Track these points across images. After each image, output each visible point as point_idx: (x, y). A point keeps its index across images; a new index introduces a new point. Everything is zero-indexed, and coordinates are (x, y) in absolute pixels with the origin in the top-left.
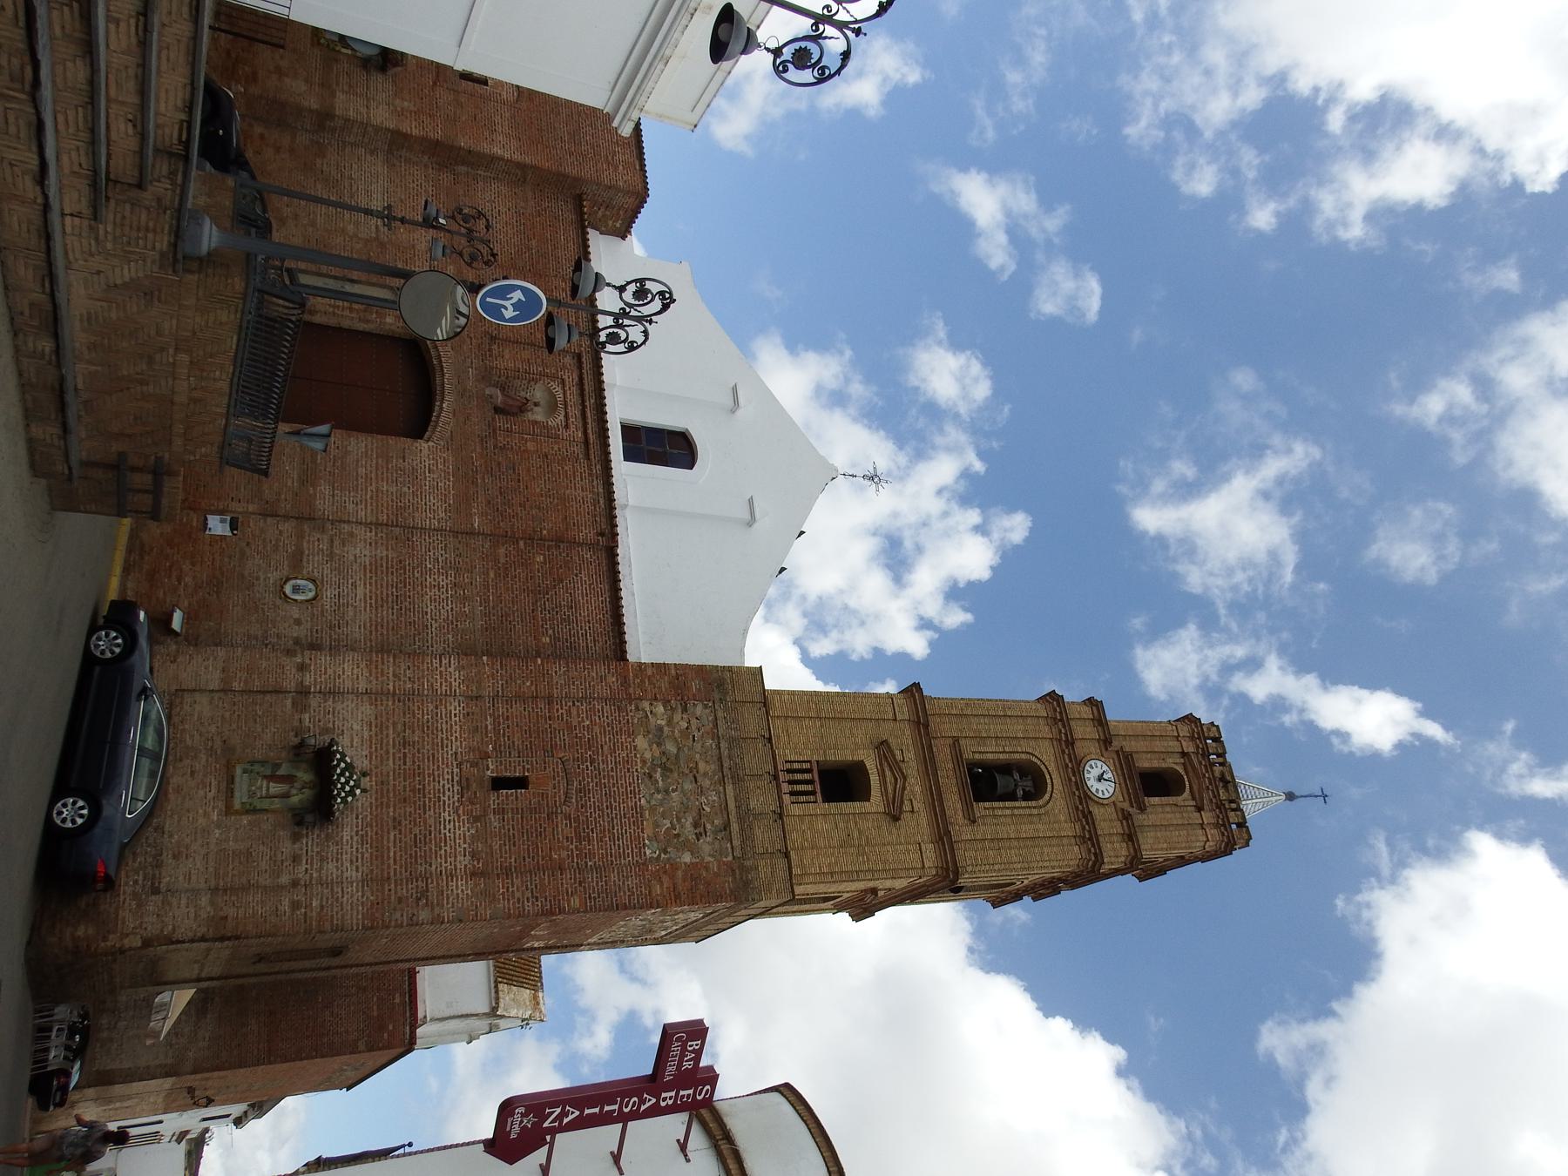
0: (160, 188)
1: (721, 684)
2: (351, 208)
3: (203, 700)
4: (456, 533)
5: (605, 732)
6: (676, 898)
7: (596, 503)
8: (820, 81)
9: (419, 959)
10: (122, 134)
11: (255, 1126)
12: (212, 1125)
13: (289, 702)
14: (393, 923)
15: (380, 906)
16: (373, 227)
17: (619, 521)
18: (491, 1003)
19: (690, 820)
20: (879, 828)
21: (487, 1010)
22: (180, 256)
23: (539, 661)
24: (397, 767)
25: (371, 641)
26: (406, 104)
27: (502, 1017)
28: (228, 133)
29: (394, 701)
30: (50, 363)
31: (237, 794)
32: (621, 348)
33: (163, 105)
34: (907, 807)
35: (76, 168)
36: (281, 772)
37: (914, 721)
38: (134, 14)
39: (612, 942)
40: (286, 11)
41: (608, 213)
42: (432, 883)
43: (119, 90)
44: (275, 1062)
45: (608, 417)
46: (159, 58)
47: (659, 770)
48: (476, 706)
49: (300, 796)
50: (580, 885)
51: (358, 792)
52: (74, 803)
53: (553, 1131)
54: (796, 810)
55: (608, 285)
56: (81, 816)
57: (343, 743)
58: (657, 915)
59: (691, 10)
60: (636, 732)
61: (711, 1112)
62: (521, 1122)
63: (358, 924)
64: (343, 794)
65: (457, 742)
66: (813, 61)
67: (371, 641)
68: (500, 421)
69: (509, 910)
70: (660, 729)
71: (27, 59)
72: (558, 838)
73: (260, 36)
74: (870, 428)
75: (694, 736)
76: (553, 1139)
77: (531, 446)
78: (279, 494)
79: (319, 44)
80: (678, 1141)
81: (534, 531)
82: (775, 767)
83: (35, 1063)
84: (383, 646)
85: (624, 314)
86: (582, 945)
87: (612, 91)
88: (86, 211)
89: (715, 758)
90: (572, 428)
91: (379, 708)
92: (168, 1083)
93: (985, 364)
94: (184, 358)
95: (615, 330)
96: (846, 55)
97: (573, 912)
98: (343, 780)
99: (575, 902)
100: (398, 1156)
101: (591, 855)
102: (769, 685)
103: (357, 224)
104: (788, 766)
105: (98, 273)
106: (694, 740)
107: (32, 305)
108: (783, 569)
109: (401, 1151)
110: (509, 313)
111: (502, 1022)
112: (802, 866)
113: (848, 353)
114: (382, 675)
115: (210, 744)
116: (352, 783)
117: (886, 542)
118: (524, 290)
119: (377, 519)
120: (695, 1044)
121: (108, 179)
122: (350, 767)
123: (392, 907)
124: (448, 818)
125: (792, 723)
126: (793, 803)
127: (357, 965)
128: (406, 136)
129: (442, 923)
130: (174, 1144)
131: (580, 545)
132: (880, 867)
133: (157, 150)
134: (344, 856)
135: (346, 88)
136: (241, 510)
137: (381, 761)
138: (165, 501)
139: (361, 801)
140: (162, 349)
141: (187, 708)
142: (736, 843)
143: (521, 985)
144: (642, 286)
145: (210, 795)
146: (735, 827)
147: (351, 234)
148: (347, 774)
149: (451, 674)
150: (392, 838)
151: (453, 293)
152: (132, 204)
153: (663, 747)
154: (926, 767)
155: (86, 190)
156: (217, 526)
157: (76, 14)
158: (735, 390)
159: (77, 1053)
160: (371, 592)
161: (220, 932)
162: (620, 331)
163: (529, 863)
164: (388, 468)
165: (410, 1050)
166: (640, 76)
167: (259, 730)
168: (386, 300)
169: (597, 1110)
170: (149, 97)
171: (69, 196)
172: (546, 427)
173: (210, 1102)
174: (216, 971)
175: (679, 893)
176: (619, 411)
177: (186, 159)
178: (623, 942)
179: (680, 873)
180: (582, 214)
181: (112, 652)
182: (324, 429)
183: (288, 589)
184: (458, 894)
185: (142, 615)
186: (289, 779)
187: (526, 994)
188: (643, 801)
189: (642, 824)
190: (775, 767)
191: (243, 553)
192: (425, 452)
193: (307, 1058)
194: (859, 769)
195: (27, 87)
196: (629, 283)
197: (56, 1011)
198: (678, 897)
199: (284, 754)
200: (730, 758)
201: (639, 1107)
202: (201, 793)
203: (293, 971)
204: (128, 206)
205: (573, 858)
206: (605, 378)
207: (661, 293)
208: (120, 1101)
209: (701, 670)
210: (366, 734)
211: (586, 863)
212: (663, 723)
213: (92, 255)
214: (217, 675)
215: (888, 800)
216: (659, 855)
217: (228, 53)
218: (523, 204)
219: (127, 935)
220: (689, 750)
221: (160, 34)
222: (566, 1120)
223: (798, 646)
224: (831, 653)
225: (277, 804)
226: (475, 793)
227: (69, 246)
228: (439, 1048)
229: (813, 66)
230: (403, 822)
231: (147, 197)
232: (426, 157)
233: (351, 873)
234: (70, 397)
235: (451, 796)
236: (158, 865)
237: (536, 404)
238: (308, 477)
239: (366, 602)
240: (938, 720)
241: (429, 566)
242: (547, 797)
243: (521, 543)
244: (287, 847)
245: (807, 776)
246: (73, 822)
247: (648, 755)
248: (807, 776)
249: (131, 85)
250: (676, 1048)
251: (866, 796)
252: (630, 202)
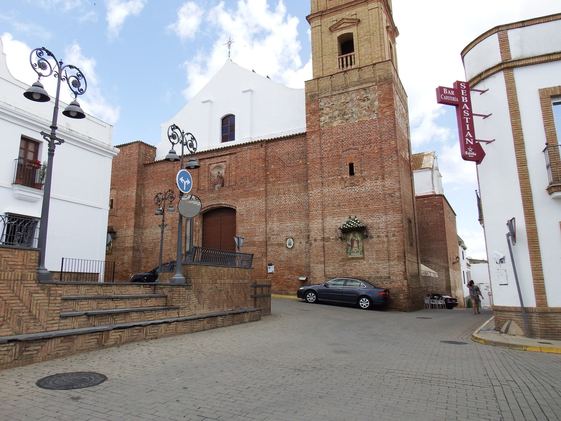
0: (166, 291)
1: (312, 96)
2: (162, 236)
3: (327, 269)
4: (266, 196)
5: (332, 138)
6: (391, 106)
7: (251, 149)
8: (83, 76)
9: (413, 195)
10: (151, 303)
11: (466, 244)
12: (465, 257)
13: (327, 243)
14: (400, 204)
15: (394, 209)
16: (167, 231)
17: (256, 140)
18: (428, 170)
19: (362, 103)
20: (363, 28)
21: (430, 171)
22: (186, 284)
23: (308, 163)
24: (347, 207)
25: (305, 220)
26: (125, 225)
27: (433, 166)
28: (145, 276)
29: (325, 210)
30: (225, 318)
31: (358, 256)
32: (194, 142)
33: (139, 293)
34: (354, 17)
35: (164, 314)
36: (350, 243)
37: (321, 17)
38: (113, 302)
39: (407, 128)
40: (103, 262)
41: (148, 155)
42: (386, 192)
43: (138, 304)
44: (446, 238)
45: (220, 147)
46: (124, 294)
47: (345, 117)
48: (325, 183)
49: (358, 237)
50: (387, 141)
51: (356, 219)
52: (361, 302)
53: (475, 140)
54: (357, 62)
55: (173, 148)
56: (365, 300)
57: (340, 225)
58: (397, 113)
59: (70, 131)
60: (331, 126)
61: (470, 83)
62: (470, 152)
63: (400, 215)
64: (357, 224)
65: (338, 188)
66: (76, 80)
67: (305, 220)
68: (227, 184)
69: (396, 165)
70: (330, 118)
71: (133, 328)
72: (370, 151)
73: (112, 270)
74: (212, 51)
75: (332, 105)
76: (477, 140)
77: (234, 173)
78: (259, 252)
79: (111, 253)
80: (480, 94)
81: (263, 169)
82: (342, 72)
83: (443, 308)
84: (306, 216)
85: (182, 142)
86: (408, 139)
87: (105, 156)
88: (177, 311)
89: (340, 96)
90: (225, 160)
91: (327, 215)
92: (451, 270)
93: (182, 6)
94: (218, 281)
95: (188, 145)
96: (71, 67)
97: (397, 143)
98: (352, 224)
99: (393, 143)
100: (480, 195)
101: (376, 138)
102: (311, 77)
103: (167, 236)
104: (341, 67)
105: (195, 306)
106: (333, 105)
107: (208, 323)
108: (268, 77)
109: (478, 194)
110: (188, 182)
111: (435, 166)
112: (378, 58)
113: (186, 63)
114: (317, 215)
115: (342, 266)
116: (353, 221)
117: (255, 39)
118: (179, 177)
119: (264, 221)
120: (445, 91)
121: (166, 306)
122: (348, 222)
123: (394, 205)
124: (364, 189)
125: (324, 67)
126: (355, 64)
127: (414, 214)
128: (135, 224)
129: (400, 188)
130: (471, 267)
131: (266, 153)
132: (378, 26)
133: (154, 293)
134: (378, 222)
135: (124, 243)
136: (265, 263)
137: (346, 212)
138: (265, 284)
139: (359, 218)
140: (217, 287)
141: (330, 273)
142: (370, 85)
143: (422, 160)
144: (171, 136)
145: (358, 264)
146: (364, 86)
147: (171, 238)
148: (350, 223)
149: (315, 193)
150: (371, 207)
151: (184, 201)
152: (172, 299)
153: (336, 116)
154: (339, 10)
155: (170, 311)
156: (271, 269)
157: (116, 317)
158: (204, 102)
159: (440, 297)
160: (289, 221)
161: (403, 257)
162: (188, 143)
163: (379, 160)
164: (247, 219)
165: (443, 196)
167: (336, 251)
168: (191, 223)
169: (468, 125)
170: (138, 296)
171: (173, 315)
172: (226, 169)
173: (458, 257)
174: (415, 258)
175: (390, 105)
176: (217, 143)
177: (155, 285)
178: (407, 124)
179: (382, 105)
180: (150, 163)
181: (314, 296)
182: (236, 239)
183: (290, 247)
184: (390, 183)
185: (301, 288)
186: (352, 241)
187: (425, 158)
188: (356, 121)
189: (365, 121)
190: (342, 72)
191: (279, 261)
192: (240, 208)
193: (445, 229)
194: (340, 38)
195: (141, 328)
196: (171, 141)
197: (426, 303)
198: (391, 105)
199: (344, 243)
200: (339, 90)
201: (467, 110)
202: (357, 267)
203: (416, 235)
204: (173, 300)
205: (377, 145)
206: (206, 150)
207: (172, 129)
208: (456, 284)
209: (307, 104)
210: (337, 218)
211: (379, 140)
212: (328, 117)
213: (190, 308)
214: (319, 265)
215: (352, 25)
216: (376, 113)
217: (120, 279)
218: (151, 184)
219: (403, 284)
220: (337, 106)
221: (118, 294)
222: (471, 136)
223: (297, 70)
224: (300, 57)
225: (361, 244)
226: (355, 181)
227: (188, 315)
228: (443, 186)
229: (78, 79)
230: (366, 204)
231: (169, 295)
232: (141, 217)
233: (383, 219)
234: (235, 312)
235: (357, 189)
236: (381, 277)
237: (219, 173)
238: (253, 244)
239: (292, 222)
240: (320, 7)
241: (278, 203)
242: (356, 156)
243: (268, 173)
244: (375, 240)
245: (344, 59)
246: (367, 302)
247: (340, 121)
248: (344, 59)
249: (135, 301)
250: (446, 98)
251: (351, 35)
252: (143, 147)
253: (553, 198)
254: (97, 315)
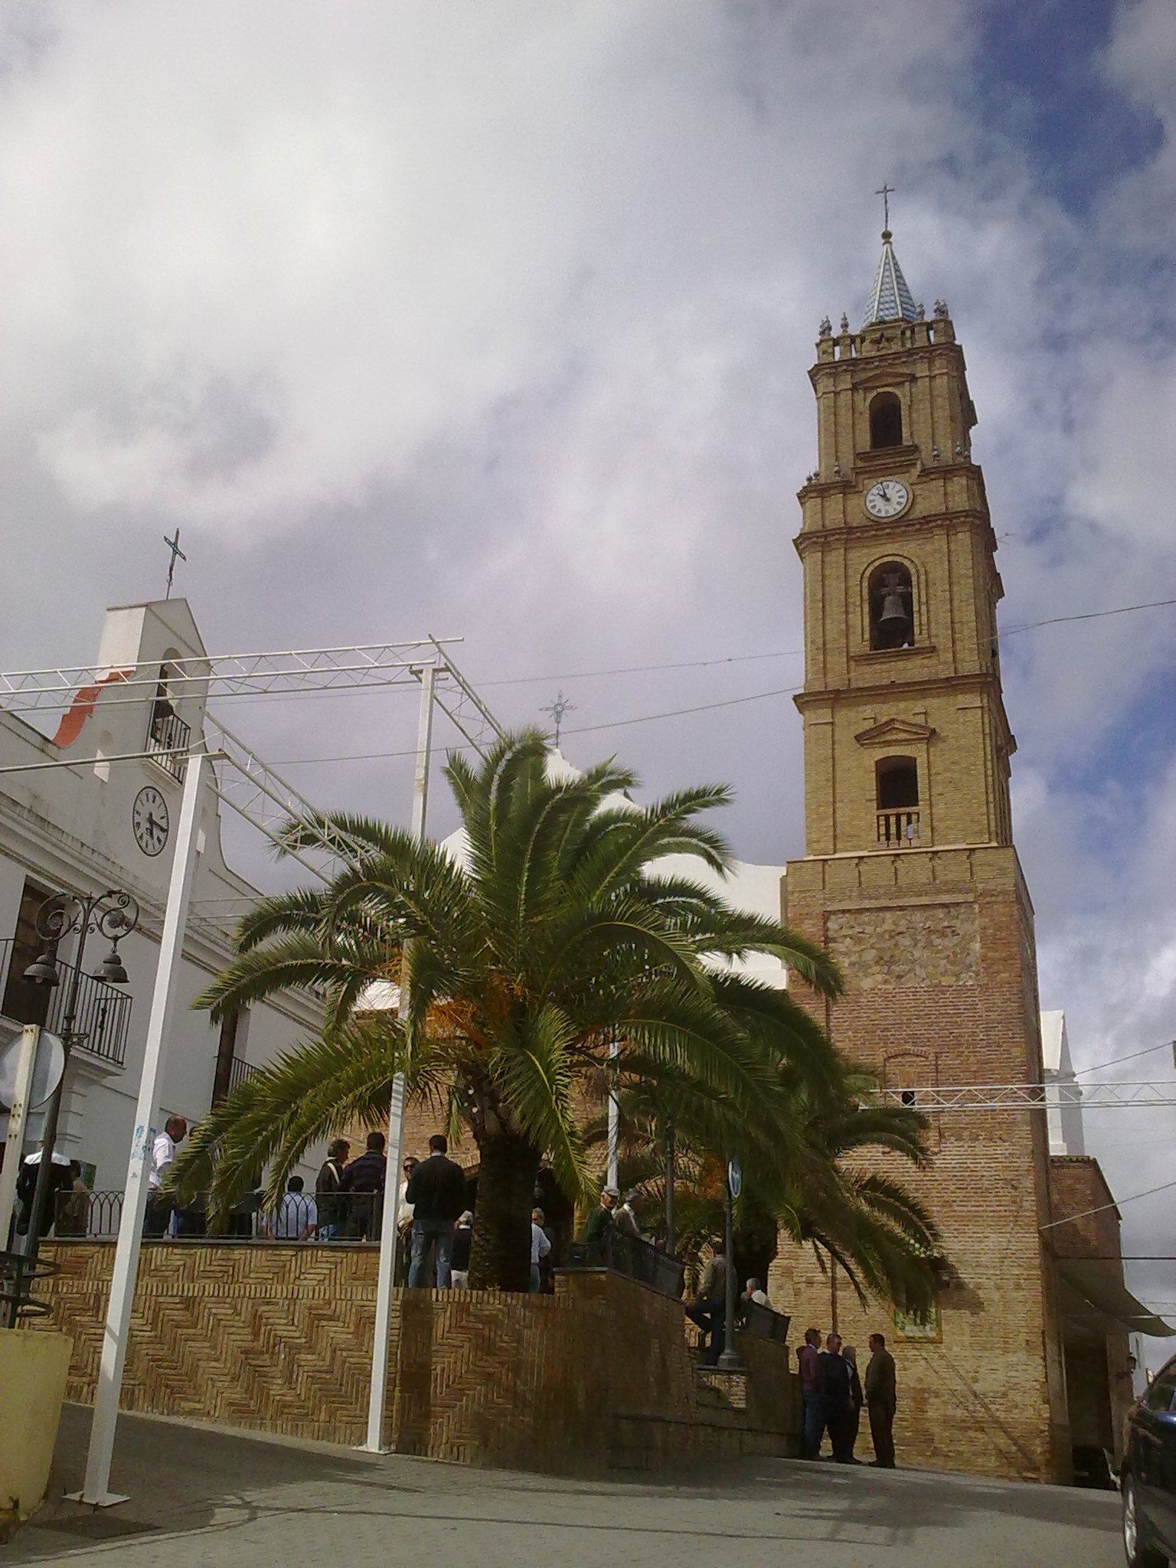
247: (879, 978)
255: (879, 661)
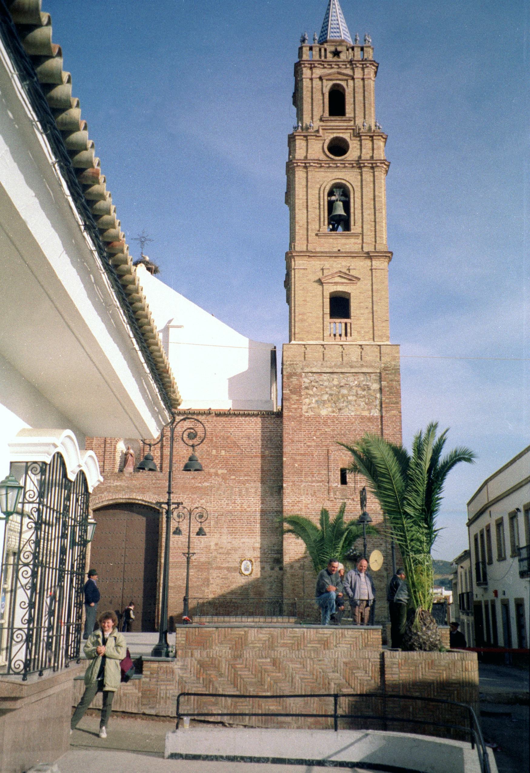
166: (13, 597)
183: (247, 573)
247: (330, 409)
253: (483, 529)
254: (314, 706)
255: (332, 237)
